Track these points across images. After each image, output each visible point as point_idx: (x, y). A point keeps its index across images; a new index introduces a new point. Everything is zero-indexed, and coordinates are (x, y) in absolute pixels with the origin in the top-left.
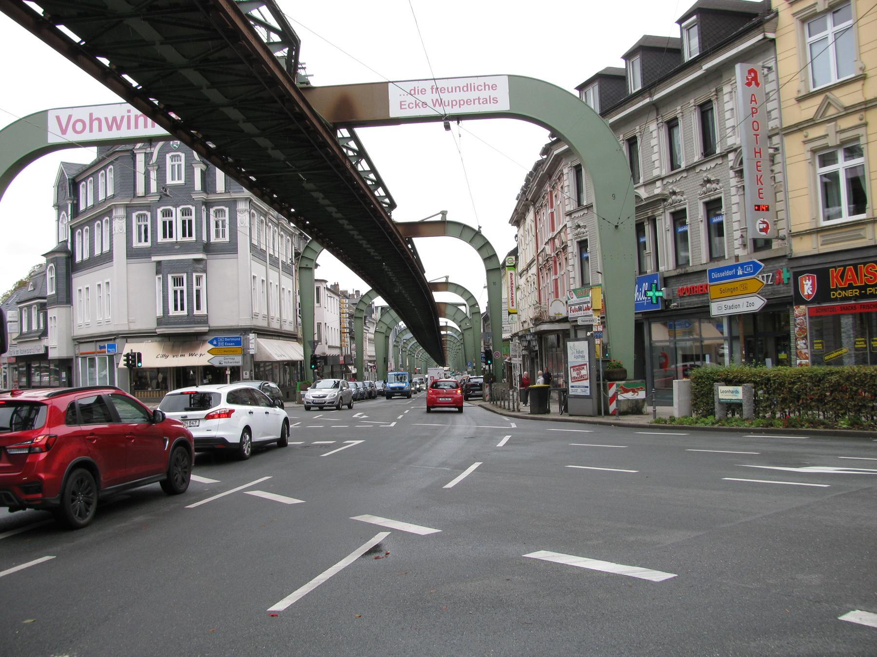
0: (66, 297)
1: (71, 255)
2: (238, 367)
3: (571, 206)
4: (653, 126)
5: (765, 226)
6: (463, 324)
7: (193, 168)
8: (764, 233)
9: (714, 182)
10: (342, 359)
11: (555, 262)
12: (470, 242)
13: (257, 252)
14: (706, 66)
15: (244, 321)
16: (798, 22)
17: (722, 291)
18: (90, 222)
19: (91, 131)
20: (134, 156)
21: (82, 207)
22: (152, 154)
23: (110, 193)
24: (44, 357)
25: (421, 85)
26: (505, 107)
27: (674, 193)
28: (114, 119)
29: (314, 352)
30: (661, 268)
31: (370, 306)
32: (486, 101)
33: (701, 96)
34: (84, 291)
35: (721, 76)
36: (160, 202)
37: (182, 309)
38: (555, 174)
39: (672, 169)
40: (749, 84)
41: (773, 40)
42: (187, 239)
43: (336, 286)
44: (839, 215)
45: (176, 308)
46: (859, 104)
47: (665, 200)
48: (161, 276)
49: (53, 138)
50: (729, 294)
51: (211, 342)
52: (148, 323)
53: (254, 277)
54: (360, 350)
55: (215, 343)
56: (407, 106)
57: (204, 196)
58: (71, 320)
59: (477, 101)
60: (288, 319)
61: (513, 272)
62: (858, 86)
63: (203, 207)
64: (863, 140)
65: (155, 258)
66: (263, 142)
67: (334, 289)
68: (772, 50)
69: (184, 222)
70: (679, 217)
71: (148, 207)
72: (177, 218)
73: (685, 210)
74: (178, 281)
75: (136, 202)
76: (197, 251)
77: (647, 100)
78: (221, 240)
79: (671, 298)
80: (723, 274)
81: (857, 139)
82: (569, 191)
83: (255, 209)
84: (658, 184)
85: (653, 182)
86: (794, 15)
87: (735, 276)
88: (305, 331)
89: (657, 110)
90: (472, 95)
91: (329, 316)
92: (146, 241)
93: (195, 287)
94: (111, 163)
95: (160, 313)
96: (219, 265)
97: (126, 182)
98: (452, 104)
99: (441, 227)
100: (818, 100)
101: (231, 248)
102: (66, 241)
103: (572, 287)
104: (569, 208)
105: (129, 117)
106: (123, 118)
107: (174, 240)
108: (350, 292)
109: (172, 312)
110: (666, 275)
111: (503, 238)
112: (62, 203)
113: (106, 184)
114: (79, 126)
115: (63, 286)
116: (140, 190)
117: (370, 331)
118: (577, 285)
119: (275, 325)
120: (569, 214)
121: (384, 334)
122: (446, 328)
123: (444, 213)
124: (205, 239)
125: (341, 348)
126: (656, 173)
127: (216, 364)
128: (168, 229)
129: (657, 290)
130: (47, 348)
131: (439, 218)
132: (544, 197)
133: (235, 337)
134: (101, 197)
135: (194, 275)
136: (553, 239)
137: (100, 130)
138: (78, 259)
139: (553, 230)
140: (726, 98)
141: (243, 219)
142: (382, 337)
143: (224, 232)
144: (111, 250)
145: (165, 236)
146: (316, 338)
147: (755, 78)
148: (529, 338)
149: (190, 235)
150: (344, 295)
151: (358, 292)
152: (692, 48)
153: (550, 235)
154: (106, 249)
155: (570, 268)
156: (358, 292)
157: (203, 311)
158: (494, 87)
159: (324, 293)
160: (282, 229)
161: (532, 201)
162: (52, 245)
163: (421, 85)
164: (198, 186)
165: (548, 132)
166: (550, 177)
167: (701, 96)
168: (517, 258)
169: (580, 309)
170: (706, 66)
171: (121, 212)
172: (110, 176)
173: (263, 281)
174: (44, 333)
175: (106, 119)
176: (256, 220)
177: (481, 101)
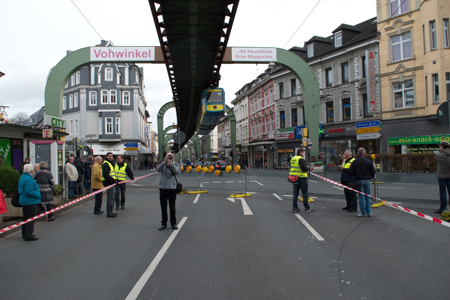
4: (320, 70)
11: (264, 119)
14: (348, 50)
15: (136, 138)
16: (389, 38)
17: (362, 131)
19: (109, 57)
20: (90, 68)
22: (99, 67)
25: (244, 49)
27: (328, 95)
28: (120, 53)
32: (268, 57)
33: (343, 60)
35: (353, 54)
36: (102, 88)
38: (268, 85)
40: (370, 58)
41: (378, 43)
42: (113, 103)
44: (402, 106)
45: (108, 132)
46: (413, 68)
47: (323, 98)
48: (102, 118)
51: (125, 145)
62: (413, 61)
64: (413, 81)
65: (99, 111)
68: (377, 46)
69: (112, 96)
72: (109, 94)
73: (333, 101)
74: (109, 120)
75: (91, 87)
76: (118, 109)
77: (319, 60)
78: (126, 104)
80: (362, 125)
81: (412, 80)
86: (387, 34)
87: (369, 126)
90: (263, 54)
93: (116, 123)
96: (126, 114)
98: (255, 57)
100: (397, 65)
101: (131, 108)
103: (276, 128)
104: (276, 99)
105: (126, 53)
106: (123, 53)
107: (108, 103)
109: (106, 133)
114: (104, 55)
116: (93, 82)
120: (276, 101)
126: (320, 87)
127: (127, 154)
128: (105, 100)
133: (132, 143)
135: (116, 118)
136: (263, 110)
139: (263, 106)
140: (355, 62)
145: (104, 102)
147: (372, 56)
148: (273, 146)
149: (115, 102)
152: (338, 43)
153: (262, 109)
155: (276, 121)
157: (119, 133)
158: (271, 52)
163: (244, 49)
164: (118, 82)
167: (343, 60)
169: (281, 136)
170: (348, 50)
171: (84, 91)
175: (116, 52)
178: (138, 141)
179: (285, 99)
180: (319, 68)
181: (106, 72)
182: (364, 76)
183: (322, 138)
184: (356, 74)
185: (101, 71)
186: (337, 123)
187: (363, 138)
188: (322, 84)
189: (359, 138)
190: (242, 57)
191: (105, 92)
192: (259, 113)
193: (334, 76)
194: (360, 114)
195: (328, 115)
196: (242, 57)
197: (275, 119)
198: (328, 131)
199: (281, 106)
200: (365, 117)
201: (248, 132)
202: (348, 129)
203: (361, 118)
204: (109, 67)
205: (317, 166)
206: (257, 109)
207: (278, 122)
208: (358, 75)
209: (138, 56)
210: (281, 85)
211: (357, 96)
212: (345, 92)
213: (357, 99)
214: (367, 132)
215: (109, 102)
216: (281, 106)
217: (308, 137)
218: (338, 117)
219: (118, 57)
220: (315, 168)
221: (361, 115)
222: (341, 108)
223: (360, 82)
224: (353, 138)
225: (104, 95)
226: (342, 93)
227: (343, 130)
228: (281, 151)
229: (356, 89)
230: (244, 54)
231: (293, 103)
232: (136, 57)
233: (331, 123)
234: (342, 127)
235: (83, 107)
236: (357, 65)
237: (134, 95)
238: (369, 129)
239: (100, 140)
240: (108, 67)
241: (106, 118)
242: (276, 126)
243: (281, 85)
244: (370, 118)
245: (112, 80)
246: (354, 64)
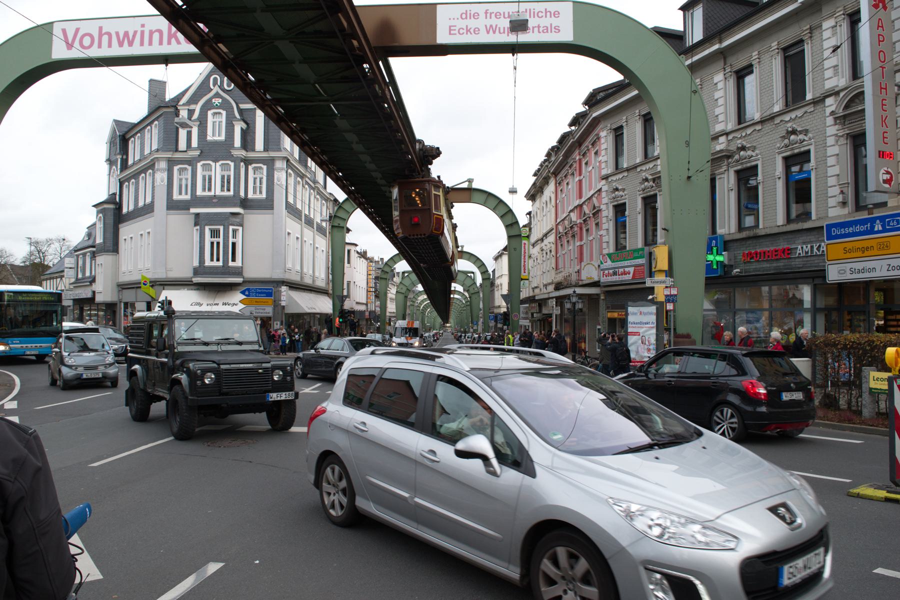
0: (113, 245)
1: (119, 206)
2: (270, 318)
3: (608, 170)
4: (719, 77)
5: (888, 176)
6: (471, 289)
8: (887, 186)
9: (801, 132)
10: (367, 314)
11: (581, 229)
12: (494, 210)
13: (293, 211)
15: (278, 275)
17: (846, 251)
18: (136, 176)
19: (100, 46)
21: (130, 162)
23: (155, 147)
24: (91, 300)
27: (743, 148)
28: (126, 34)
29: (342, 306)
30: (720, 231)
31: (392, 271)
32: (546, 30)
33: (788, 36)
35: (820, 10)
36: (201, 157)
39: (740, 123)
42: (226, 193)
43: (365, 253)
45: (212, 260)
47: (728, 157)
48: (198, 227)
50: (859, 254)
51: (243, 293)
53: (289, 234)
54: (384, 307)
55: (247, 293)
56: (456, 32)
57: (243, 153)
58: (117, 266)
59: (536, 30)
61: (526, 242)
63: (242, 164)
65: (193, 210)
66: (288, 49)
67: (363, 255)
69: (223, 177)
70: (746, 175)
71: (192, 162)
75: (178, 155)
76: (234, 206)
78: (258, 196)
79: (732, 263)
82: (606, 154)
83: (292, 170)
84: (722, 139)
85: (715, 138)
87: (871, 231)
88: (336, 288)
89: (725, 58)
92: (186, 194)
93: (231, 240)
94: (157, 119)
95: (196, 263)
96: (255, 220)
97: (170, 140)
101: (267, 205)
102: (115, 194)
103: (605, 252)
105: (143, 33)
106: (135, 33)
107: (212, 193)
108: (376, 259)
109: (208, 263)
110: (727, 238)
111: (521, 208)
112: (113, 159)
113: (152, 139)
114: (87, 41)
115: (110, 235)
116: (182, 145)
117: (392, 292)
118: (612, 249)
119: (308, 281)
120: (606, 178)
121: (405, 295)
122: (455, 292)
123: (470, 181)
124: (242, 194)
125: (367, 304)
126: (719, 128)
128: (208, 183)
130: (94, 292)
131: (465, 185)
134: (147, 151)
135: (231, 228)
136: (580, 206)
137: (110, 46)
138: (125, 210)
139: (580, 197)
140: (826, 34)
141: (280, 176)
142: (401, 297)
143: (260, 188)
145: (204, 190)
146: (345, 293)
148: (574, 299)
150: (371, 260)
151: (382, 259)
153: (577, 202)
155: (603, 232)
156: (382, 259)
157: (238, 263)
159: (354, 255)
160: (318, 194)
161: (553, 173)
162: (104, 197)
163: (474, 8)
164: (237, 142)
165: (452, 210)
166: (580, 145)
167: (788, 36)
168: (530, 229)
169: (615, 274)
171: (163, 165)
172: (155, 131)
173: (297, 238)
174: (93, 280)
176: (291, 181)
177: (541, 29)
178: (283, 283)
180: (717, 72)
182: (856, 73)
183: (718, 280)
184: (828, 74)
185: (199, 119)
186: (769, 231)
187: (849, 277)
188: (723, 116)
189: (834, 274)
190: (468, 31)
191: (206, 167)
194: (840, 198)
195: (742, 207)
196: (468, 31)
197: (602, 229)
199: (617, 189)
200: (858, 207)
201: (554, 266)
202: (801, 248)
203: (845, 211)
204: (217, 107)
206: (569, 205)
208: (836, 74)
209: (173, 40)
210: (618, 133)
211: (831, 141)
212: (794, 132)
214: (864, 252)
215: (217, 190)
216: (617, 189)
217: (669, 273)
218: (774, 210)
219: (121, 44)
221: (844, 204)
222: (780, 186)
223: (842, 94)
224: (816, 277)
225: (205, 173)
226: (783, 137)
227: (788, 251)
228: (615, 315)
229: (830, 120)
230: (472, 23)
231: (646, 180)
232: (169, 43)
234: (782, 245)
235: (161, 204)
237: (276, 174)
238: (873, 243)
239: (197, 280)
241: (207, 229)
242: (605, 245)
243: (618, 133)
244: (877, 213)
245: (223, 138)
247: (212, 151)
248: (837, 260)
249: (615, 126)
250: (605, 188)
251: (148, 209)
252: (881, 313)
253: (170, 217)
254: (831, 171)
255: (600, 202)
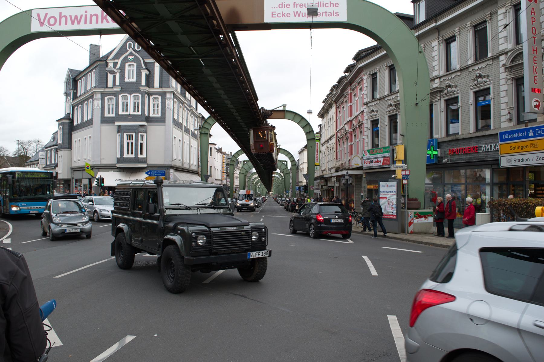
0: (68, 145)
1: (72, 121)
3: (368, 99)
4: (435, 43)
5: (537, 103)
7: (141, 72)
8: (536, 109)
9: (484, 77)
11: (351, 135)
13: (177, 124)
17: (511, 148)
19: (60, 24)
21: (79, 94)
23: (93, 85)
26: (343, 18)
27: (450, 86)
30: (435, 136)
31: (237, 160)
32: (330, 14)
33: (477, 18)
34: (78, 141)
36: (122, 91)
37: (132, 153)
39: (447, 71)
42: (136, 113)
43: (221, 149)
45: (128, 153)
47: (441, 91)
48: (120, 134)
49: (35, 28)
50: (520, 150)
51: (147, 173)
52: (111, 160)
53: (175, 138)
54: (232, 182)
55: (149, 173)
56: (276, 16)
57: (147, 89)
59: (324, 14)
60: (194, 163)
63: (146, 95)
69: (135, 103)
71: (116, 94)
73: (457, 97)
75: (107, 90)
76: (142, 121)
78: (156, 115)
79: (443, 156)
83: (177, 99)
84: (437, 81)
85: (433, 80)
87: (527, 137)
91: (216, 163)
93: (140, 141)
95: (119, 156)
96: (154, 129)
97: (103, 81)
99: (282, 113)
101: (162, 120)
102: (69, 114)
103: (366, 149)
104: (365, 101)
105: (86, 16)
106: (82, 16)
107: (128, 113)
108: (227, 153)
109: (126, 155)
110: (440, 141)
111: (315, 122)
112: (68, 92)
113: (92, 80)
114: (52, 21)
115: (66, 138)
116: (110, 84)
117: (237, 173)
118: (370, 147)
119: (186, 166)
120: (366, 104)
121: (245, 174)
123: (284, 106)
124: (146, 114)
125: (222, 180)
126: (435, 74)
129: (434, 150)
131: (281, 108)
132: (345, 97)
135: (140, 134)
137: (66, 24)
138: (75, 124)
139: (351, 116)
140: (500, 17)
141: (169, 103)
144: (92, 119)
146: (209, 174)
148: (347, 177)
150: (224, 154)
151: (231, 153)
153: (349, 119)
154: (90, 117)
155: (364, 137)
156: (231, 153)
157: (144, 155)
159: (214, 151)
160: (192, 113)
162: (63, 115)
164: (143, 82)
166: (351, 84)
167: (477, 18)
168: (321, 135)
169: (372, 162)
171: (98, 96)
172: (94, 76)
173: (180, 140)
176: (176, 106)
177: (327, 14)
179: (380, 99)
180: (434, 40)
181: (127, 68)
182: (518, 40)
184: (501, 41)
185: (120, 68)
186: (465, 137)
187: (513, 164)
188: (437, 67)
189: (504, 162)
190: (283, 15)
191: (125, 97)
192: (346, 126)
193: (463, 50)
196: (283, 15)
198: (447, 152)
199: (373, 111)
200: (519, 122)
202: (484, 147)
203: (511, 124)
204: (131, 61)
205: (420, 217)
207: (368, 138)
208: (506, 41)
209: (105, 21)
210: (374, 77)
211: (503, 82)
212: (480, 76)
213: (504, 88)
215: (131, 111)
216: (373, 111)
217: (405, 161)
218: (466, 125)
219: (73, 23)
220: (416, 221)
221: (510, 120)
222: (472, 109)
223: (509, 54)
224: (494, 164)
226: (474, 80)
227: (476, 149)
228: (372, 187)
229: (502, 70)
230: (286, 10)
231: (391, 105)
232: (102, 22)
233: (454, 138)
234: (473, 145)
235: (97, 120)
236: (504, 22)
238: (528, 144)
239: (119, 165)
240: (129, 61)
241: (125, 135)
242: (365, 145)
243: (374, 77)
244: (531, 126)
245: (134, 80)
246: (498, 21)
247: (128, 88)
248: (506, 154)
249: (372, 73)
250: (366, 110)
251: (90, 123)
252: (533, 186)
253: (102, 127)
254: (503, 100)
255: (363, 119)
